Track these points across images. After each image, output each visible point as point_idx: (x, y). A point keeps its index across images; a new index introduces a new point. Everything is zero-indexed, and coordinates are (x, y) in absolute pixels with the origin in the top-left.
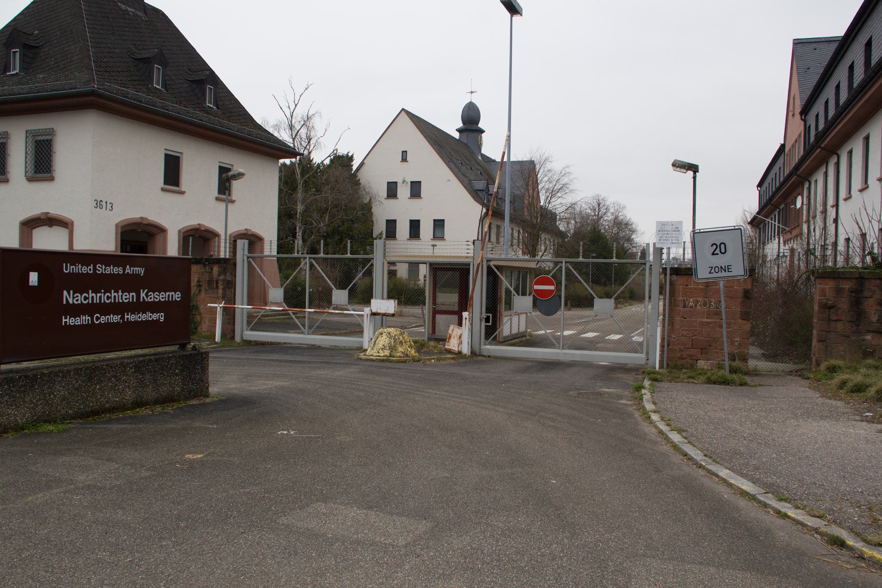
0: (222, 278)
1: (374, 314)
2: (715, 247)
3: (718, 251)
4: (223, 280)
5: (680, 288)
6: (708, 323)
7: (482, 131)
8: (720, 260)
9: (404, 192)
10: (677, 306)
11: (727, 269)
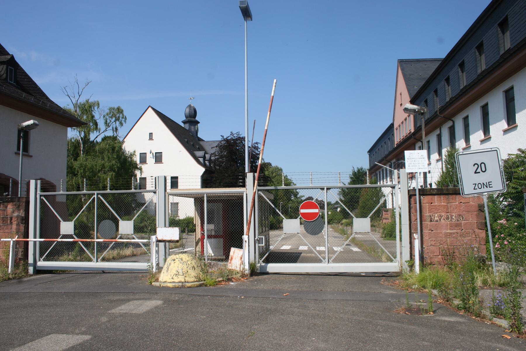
0: (16, 214)
1: (159, 241)
2: (476, 166)
3: (479, 170)
4: (18, 217)
5: (426, 206)
6: (451, 233)
7: (198, 122)
8: (482, 178)
9: (150, 159)
10: (425, 221)
11: (488, 185)
